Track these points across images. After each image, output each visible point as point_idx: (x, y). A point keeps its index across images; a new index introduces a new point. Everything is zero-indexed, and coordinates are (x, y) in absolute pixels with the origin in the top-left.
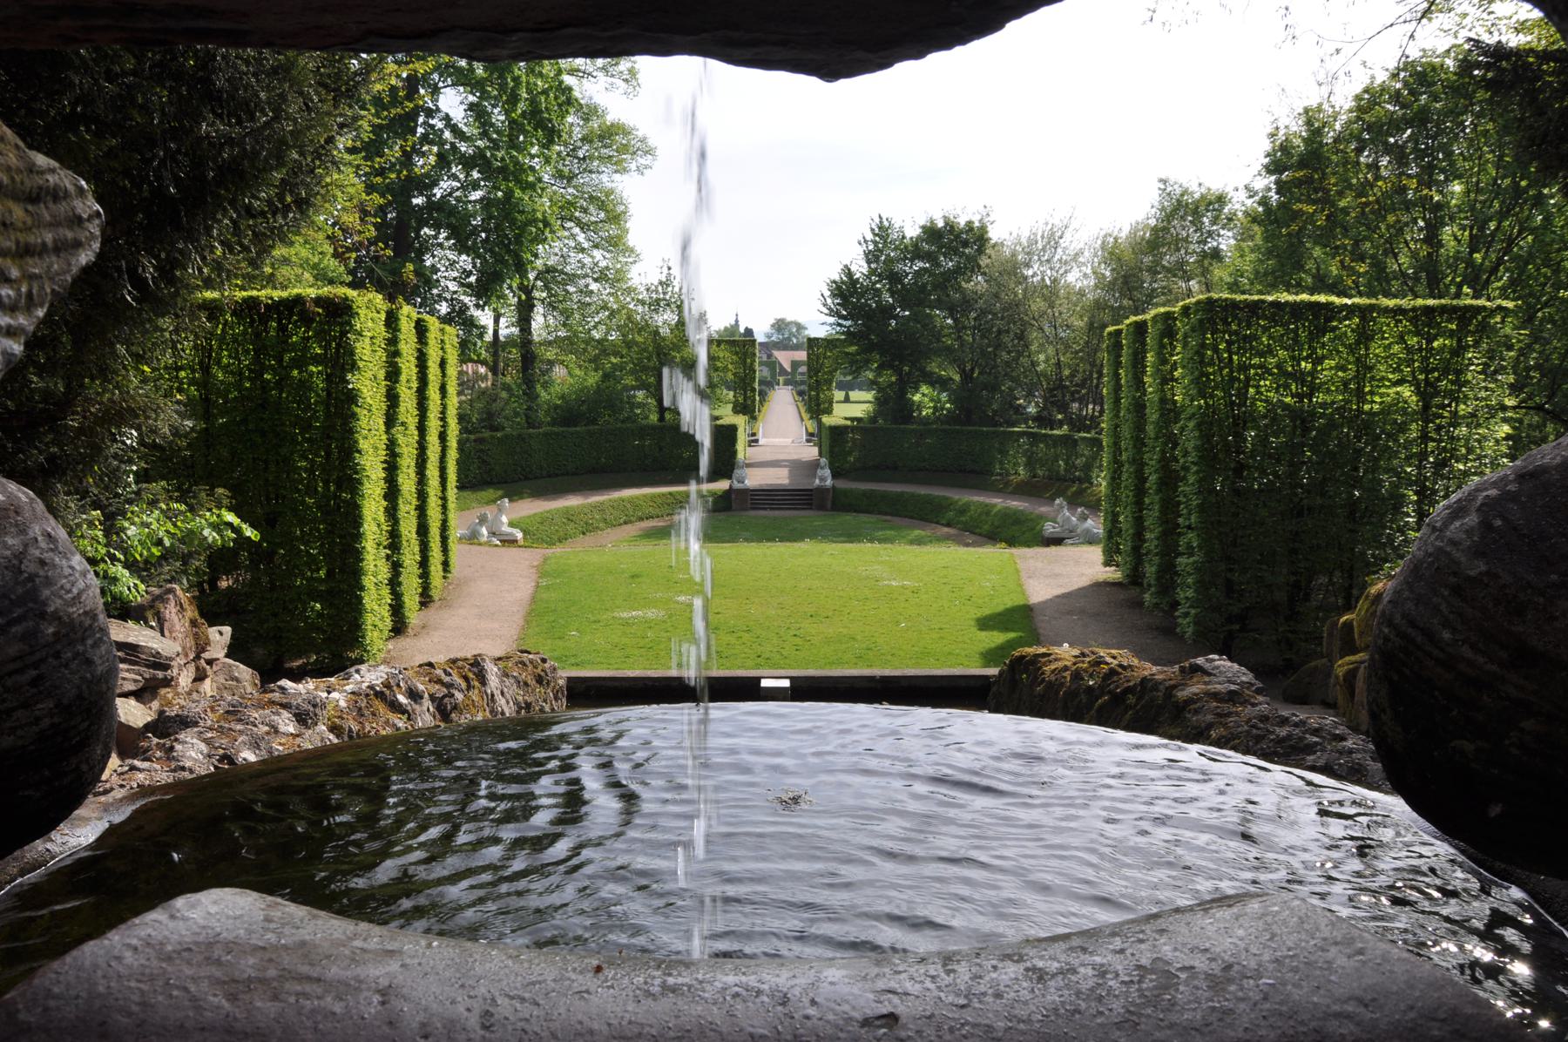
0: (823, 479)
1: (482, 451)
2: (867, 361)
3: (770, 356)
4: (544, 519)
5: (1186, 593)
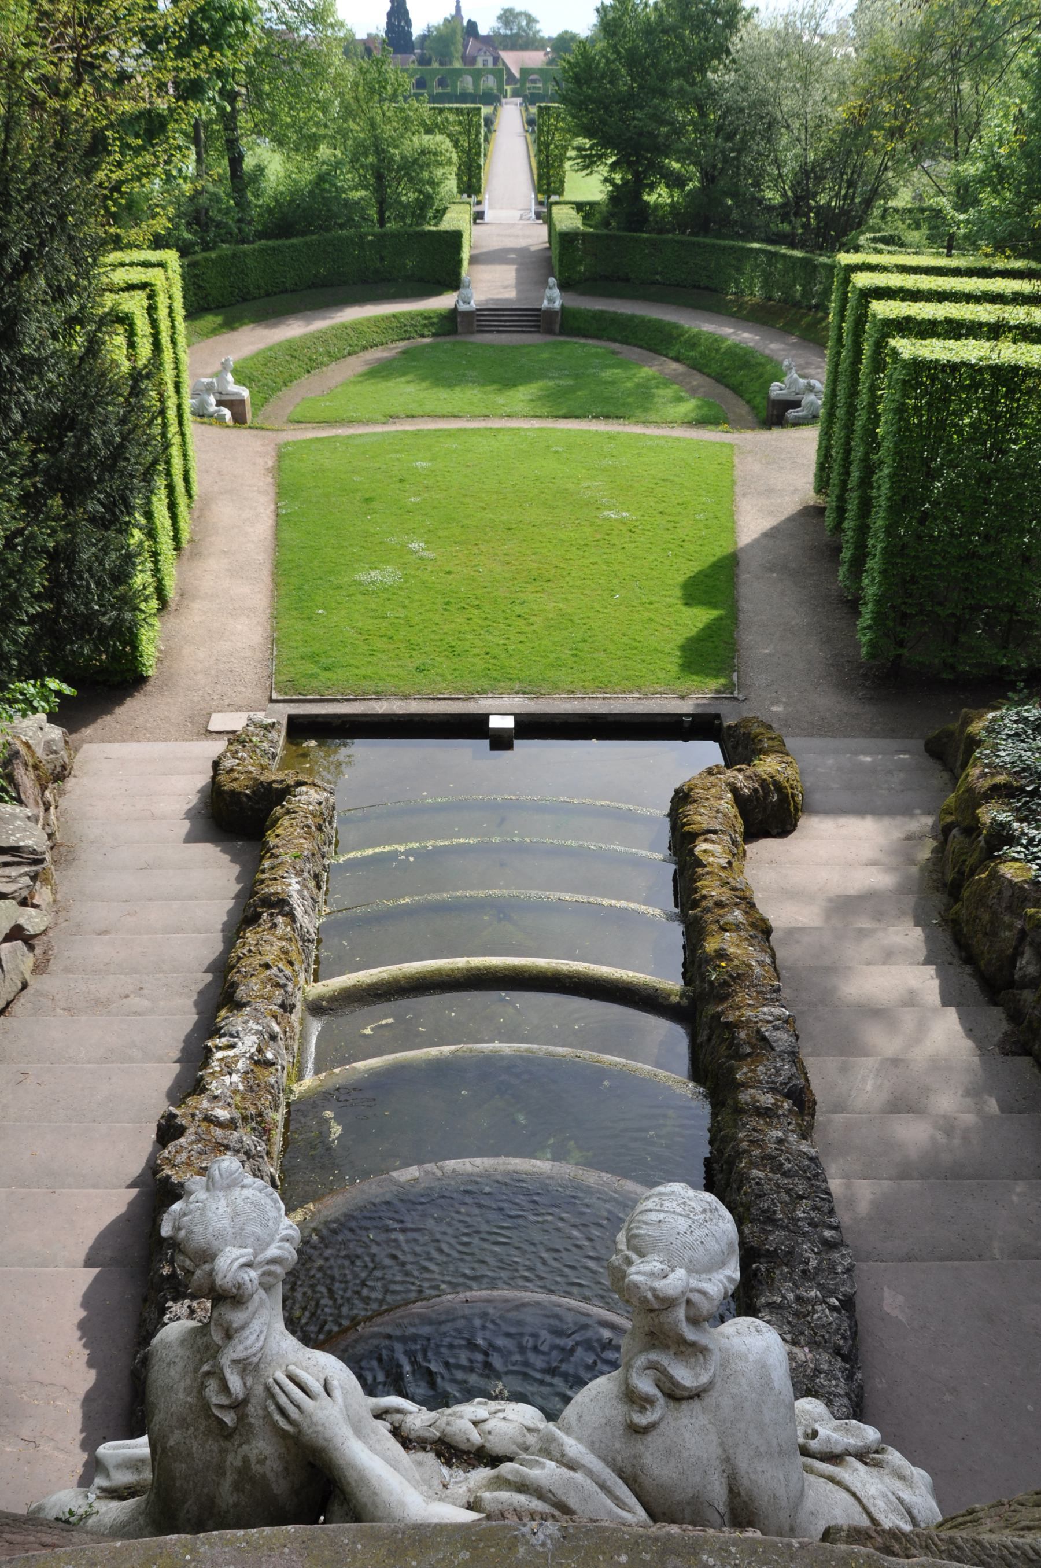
0: (551, 300)
1: (196, 276)
3: (496, 59)
4: (268, 358)
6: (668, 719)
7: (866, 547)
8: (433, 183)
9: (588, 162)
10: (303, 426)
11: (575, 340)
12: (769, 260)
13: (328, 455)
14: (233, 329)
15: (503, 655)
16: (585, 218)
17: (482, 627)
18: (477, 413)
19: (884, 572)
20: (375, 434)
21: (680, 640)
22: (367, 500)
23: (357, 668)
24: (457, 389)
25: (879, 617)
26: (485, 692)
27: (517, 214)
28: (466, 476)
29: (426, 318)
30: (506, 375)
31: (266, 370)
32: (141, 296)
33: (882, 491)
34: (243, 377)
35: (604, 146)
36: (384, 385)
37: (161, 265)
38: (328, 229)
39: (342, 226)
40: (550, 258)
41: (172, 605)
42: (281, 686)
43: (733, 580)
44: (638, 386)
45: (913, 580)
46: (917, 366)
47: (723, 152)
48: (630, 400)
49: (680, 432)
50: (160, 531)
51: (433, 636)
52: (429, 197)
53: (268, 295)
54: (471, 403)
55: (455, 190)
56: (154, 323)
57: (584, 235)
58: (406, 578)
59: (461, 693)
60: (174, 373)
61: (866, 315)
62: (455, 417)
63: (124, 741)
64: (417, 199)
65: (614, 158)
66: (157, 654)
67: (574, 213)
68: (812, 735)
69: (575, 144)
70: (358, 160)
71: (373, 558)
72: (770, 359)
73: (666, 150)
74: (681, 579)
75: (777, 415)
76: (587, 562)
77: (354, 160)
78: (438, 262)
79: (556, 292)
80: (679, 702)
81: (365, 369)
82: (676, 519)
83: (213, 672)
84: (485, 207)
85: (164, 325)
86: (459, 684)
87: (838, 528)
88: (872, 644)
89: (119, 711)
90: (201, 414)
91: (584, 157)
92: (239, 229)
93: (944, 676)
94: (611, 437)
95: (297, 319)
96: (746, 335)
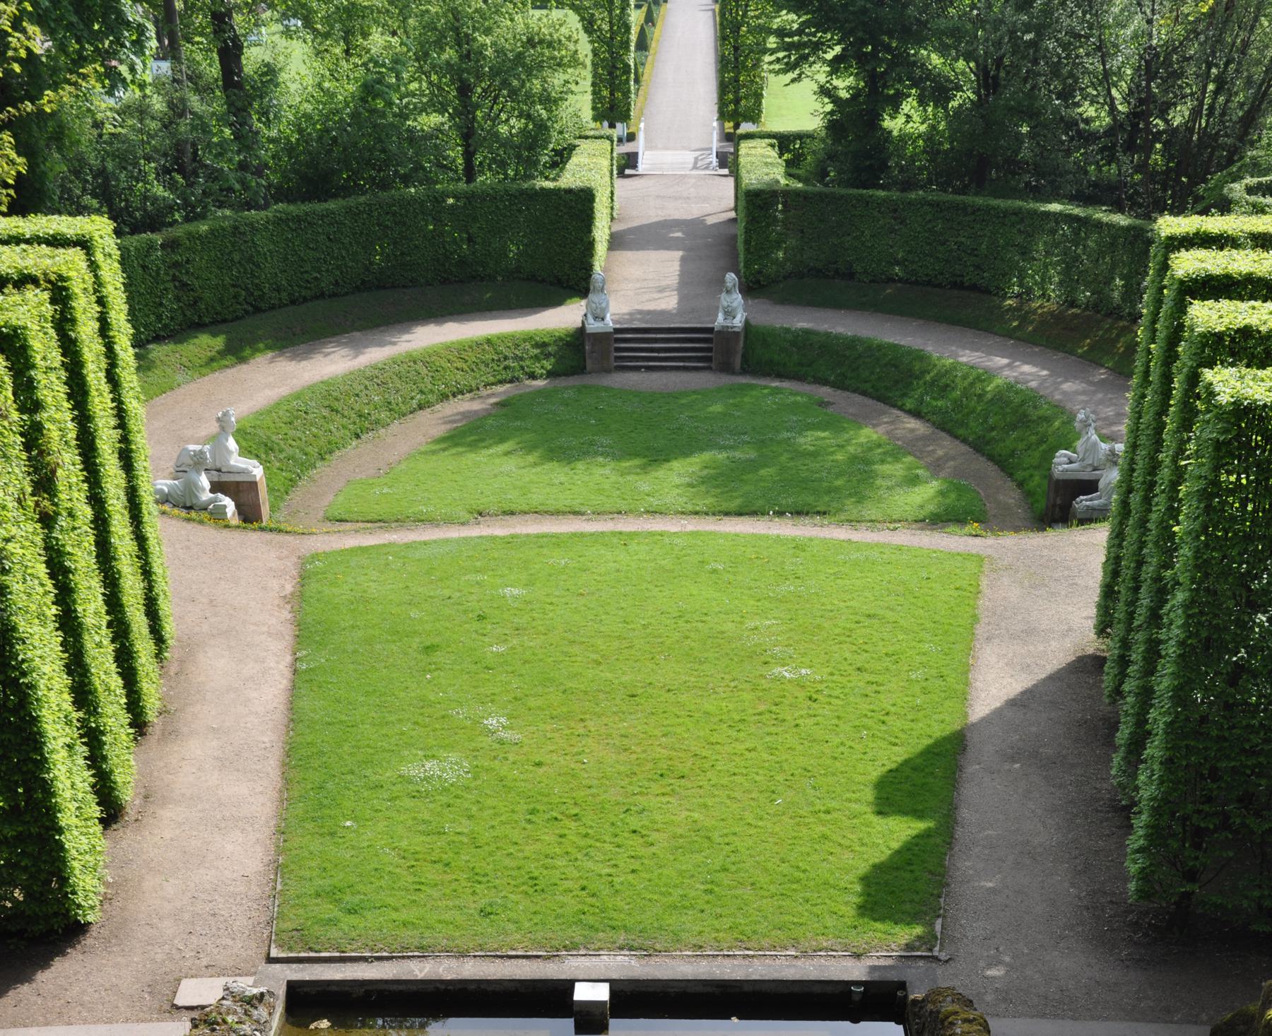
1: (176, 265)
2: (817, 47)
4: (295, 411)
5: (1154, 750)
6: (829, 989)
7: (1146, 721)
8: (549, 101)
9: (798, 56)
10: (348, 526)
11: (762, 382)
12: (1076, 232)
13: (374, 575)
14: (242, 360)
15: (607, 891)
16: (789, 163)
17: (580, 849)
18: (608, 507)
19: (1168, 763)
20: (447, 540)
21: (863, 868)
22: (429, 649)
23: (396, 910)
24: (580, 465)
25: (1156, 834)
26: (576, 948)
27: (690, 157)
28: (577, 611)
29: (537, 345)
30: (652, 445)
31: (291, 433)
32: (37, 298)
33: (1173, 633)
34: (253, 444)
35: (821, 27)
36: (472, 458)
37: (84, 244)
38: (385, 185)
39: (407, 180)
40: (734, 237)
41: (131, 812)
42: (285, 941)
43: (953, 776)
44: (854, 459)
45: (1215, 775)
46: (1243, 412)
47: (1012, 33)
48: (839, 483)
49: (905, 538)
50: (102, 696)
51: (507, 862)
52: (542, 127)
53: (293, 302)
54: (600, 491)
55: (587, 114)
56: (69, 347)
57: (787, 193)
58: (476, 772)
59: (542, 947)
60: (116, 434)
61: (1181, 327)
62: (576, 513)
63: (47, 1024)
64: (523, 131)
65: (838, 49)
66: (102, 889)
67: (773, 153)
68: (1043, 1016)
69: (776, 23)
70: (426, 54)
71: (432, 742)
72: (1059, 408)
73: (915, 33)
74: (875, 773)
75: (1059, 506)
76: (740, 747)
77: (422, 56)
78: (554, 247)
79: (737, 299)
80: (850, 963)
81: (441, 430)
82: (879, 679)
83: (187, 917)
84: (640, 146)
85: (92, 352)
86: (539, 936)
87: (1118, 692)
88: (1144, 876)
89: (41, 976)
90: (183, 504)
91: (788, 47)
92: (243, 182)
93: (1255, 927)
94: (799, 546)
95: (339, 344)
96: (1027, 368)
